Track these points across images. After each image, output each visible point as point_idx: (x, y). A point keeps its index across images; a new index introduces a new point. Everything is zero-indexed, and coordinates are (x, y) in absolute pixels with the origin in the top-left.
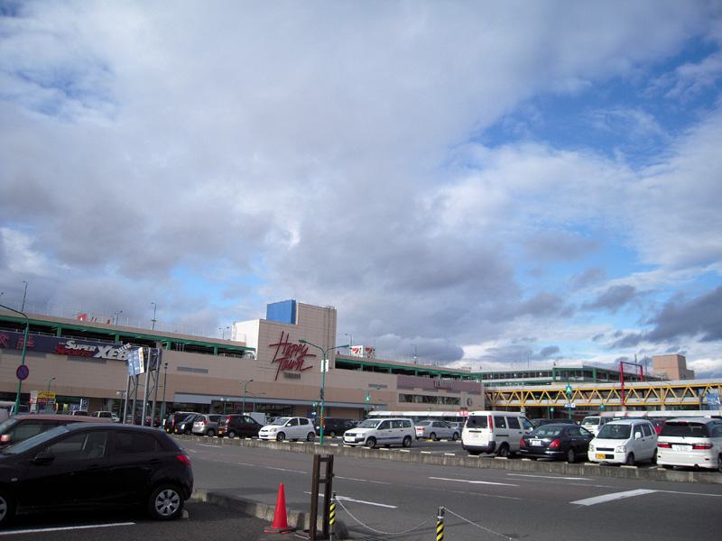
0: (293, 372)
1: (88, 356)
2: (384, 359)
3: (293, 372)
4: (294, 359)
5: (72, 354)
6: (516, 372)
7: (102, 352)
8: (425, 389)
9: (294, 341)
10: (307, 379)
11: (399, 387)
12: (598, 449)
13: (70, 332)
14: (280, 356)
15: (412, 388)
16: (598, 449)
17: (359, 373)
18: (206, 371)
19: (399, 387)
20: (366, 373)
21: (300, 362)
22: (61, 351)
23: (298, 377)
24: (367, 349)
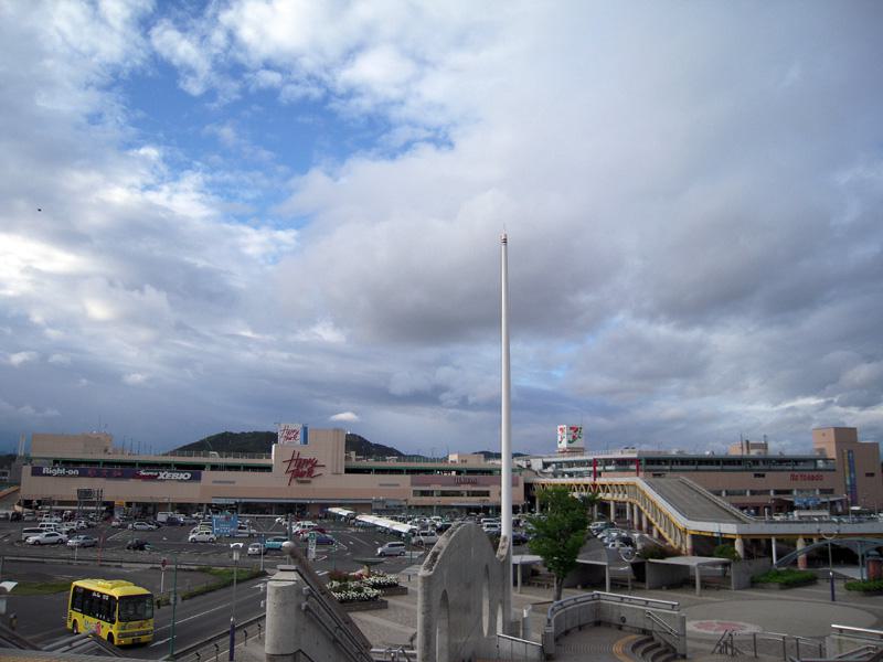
0: (305, 479)
1: (153, 478)
2: (693, 454)
3: (305, 479)
4: (306, 470)
5: (144, 478)
6: (89, 476)
7: (162, 476)
8: (443, 485)
9: (305, 456)
10: (317, 484)
11: (412, 484)
12: (268, 468)
13: (144, 465)
14: (292, 468)
15: (429, 485)
16: (268, 468)
17: (372, 476)
18: (233, 482)
19: (412, 484)
20: (246, 473)
21: (310, 473)
22: (137, 476)
23: (309, 482)
24: (571, 428)
